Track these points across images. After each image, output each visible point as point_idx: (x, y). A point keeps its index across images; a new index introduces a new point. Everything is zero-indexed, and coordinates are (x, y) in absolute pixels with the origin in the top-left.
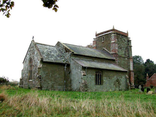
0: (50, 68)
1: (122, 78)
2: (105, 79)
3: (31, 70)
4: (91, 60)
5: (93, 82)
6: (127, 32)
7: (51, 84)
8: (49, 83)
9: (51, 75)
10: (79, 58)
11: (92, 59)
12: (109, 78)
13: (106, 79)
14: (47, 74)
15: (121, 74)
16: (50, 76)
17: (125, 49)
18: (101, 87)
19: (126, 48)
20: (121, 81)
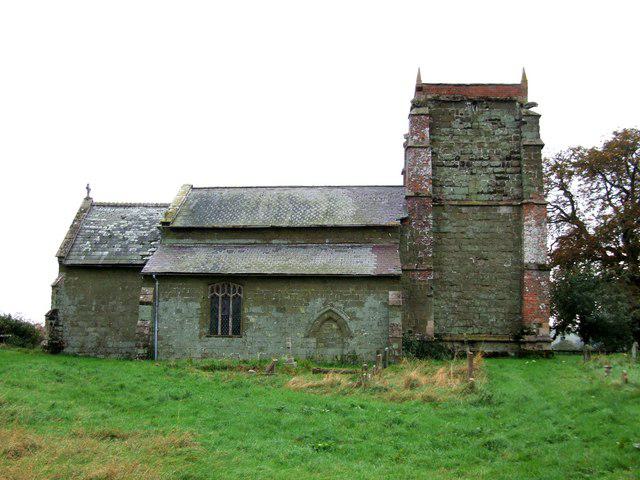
0: (91, 282)
1: (361, 304)
2: (253, 315)
3: (364, 261)
4: (245, 241)
5: (194, 327)
6: (525, 80)
7: (96, 334)
8: (88, 334)
9: (97, 306)
10: (196, 241)
11: (259, 239)
12: (281, 310)
13: (259, 315)
14: (80, 303)
15: (357, 288)
16: (93, 309)
17: (498, 163)
18: (234, 344)
19: (508, 158)
20: (357, 319)
